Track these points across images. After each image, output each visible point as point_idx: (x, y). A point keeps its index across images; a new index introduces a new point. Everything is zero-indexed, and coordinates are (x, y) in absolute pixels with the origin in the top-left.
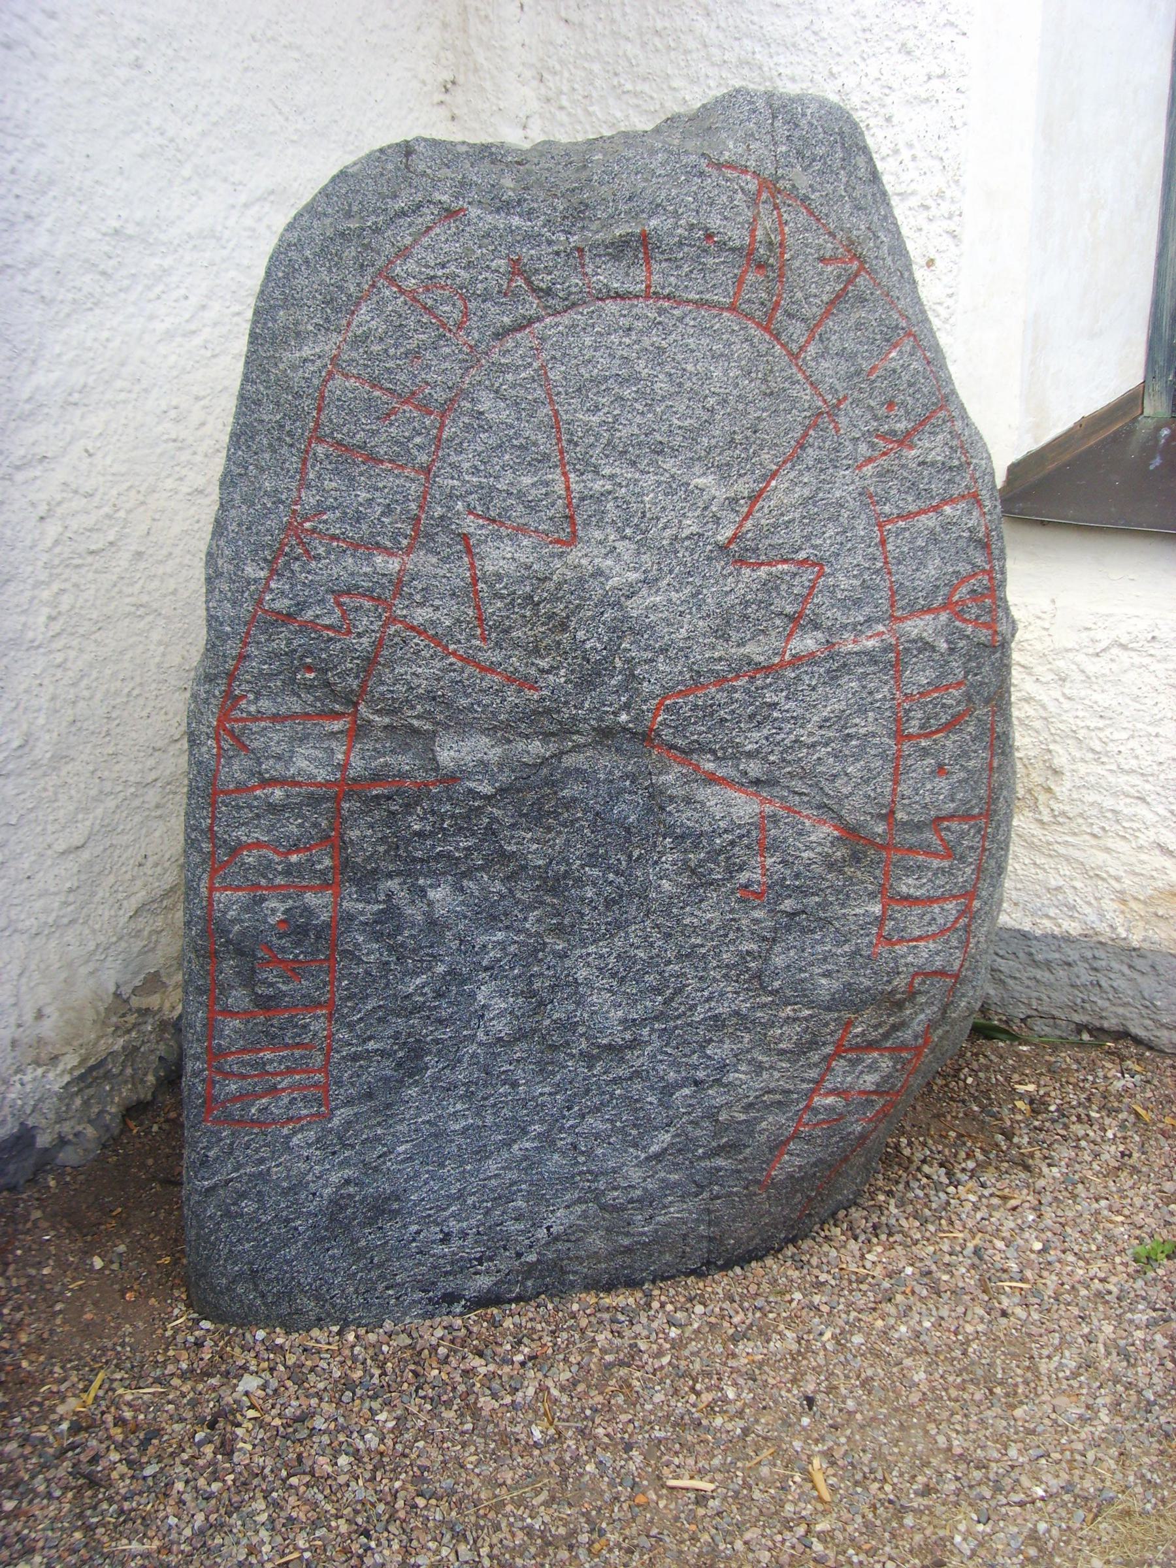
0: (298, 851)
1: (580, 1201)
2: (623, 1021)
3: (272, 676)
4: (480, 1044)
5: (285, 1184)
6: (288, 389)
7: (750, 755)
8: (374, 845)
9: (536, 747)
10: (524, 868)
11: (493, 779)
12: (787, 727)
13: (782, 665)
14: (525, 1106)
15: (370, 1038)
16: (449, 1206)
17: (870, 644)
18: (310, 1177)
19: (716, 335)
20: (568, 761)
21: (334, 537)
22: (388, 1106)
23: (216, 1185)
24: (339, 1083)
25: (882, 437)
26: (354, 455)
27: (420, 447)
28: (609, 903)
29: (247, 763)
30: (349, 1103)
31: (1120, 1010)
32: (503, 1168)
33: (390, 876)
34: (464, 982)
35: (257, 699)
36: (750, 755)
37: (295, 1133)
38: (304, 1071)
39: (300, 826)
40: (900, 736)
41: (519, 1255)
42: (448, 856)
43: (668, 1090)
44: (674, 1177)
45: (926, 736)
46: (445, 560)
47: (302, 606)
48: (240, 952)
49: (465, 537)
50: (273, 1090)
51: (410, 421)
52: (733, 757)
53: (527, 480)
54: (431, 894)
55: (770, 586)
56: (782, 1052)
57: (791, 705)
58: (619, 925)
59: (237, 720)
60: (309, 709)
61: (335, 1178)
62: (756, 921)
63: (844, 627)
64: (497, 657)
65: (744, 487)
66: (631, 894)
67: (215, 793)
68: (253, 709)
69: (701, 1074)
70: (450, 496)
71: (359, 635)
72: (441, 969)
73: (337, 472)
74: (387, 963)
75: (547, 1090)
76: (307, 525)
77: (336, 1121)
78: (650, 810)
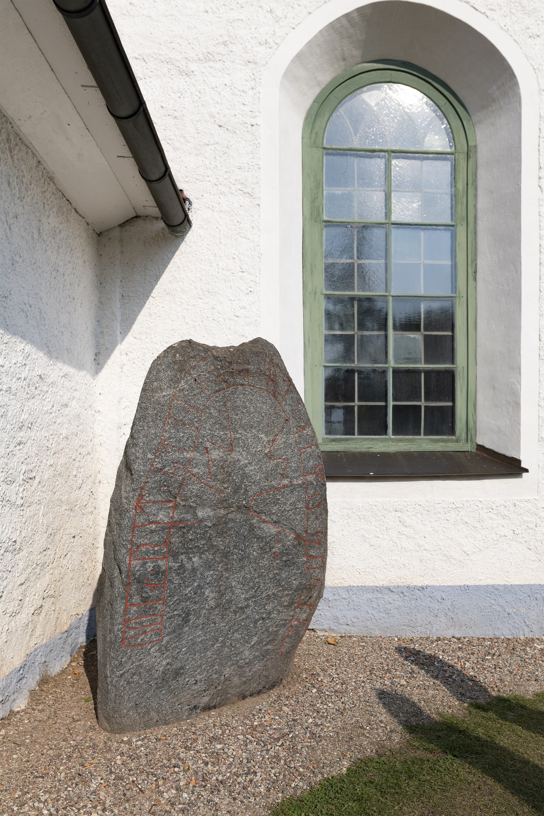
0: (157, 546)
1: (233, 665)
2: (245, 598)
3: (154, 488)
4: (207, 609)
5: (148, 668)
6: (159, 404)
7: (273, 514)
8: (178, 543)
9: (222, 511)
10: (218, 550)
11: (211, 521)
12: (282, 505)
13: (280, 488)
14: (217, 631)
15: (176, 610)
16: (197, 669)
17: (300, 482)
18: (156, 664)
19: (263, 397)
20: (230, 516)
21: (173, 446)
22: (180, 634)
23: (124, 672)
24: (165, 628)
25: (299, 427)
26: (178, 424)
27: (196, 422)
28: (240, 560)
29: (145, 517)
30: (168, 635)
31: (327, 622)
32: (212, 654)
33: (182, 554)
34: (202, 589)
35: (149, 496)
36: (273, 514)
37: (152, 647)
38: (155, 624)
39: (159, 538)
40: (308, 508)
41: (216, 687)
42: (198, 547)
43: (256, 622)
44: (257, 654)
45: (313, 508)
46: (202, 455)
47: (164, 467)
48: (139, 582)
49: (207, 448)
50: (145, 632)
51: (194, 414)
52: (270, 515)
53: (222, 433)
54: (194, 559)
55: (277, 465)
56: (285, 606)
57: (283, 499)
58: (242, 568)
59: (142, 503)
60: (163, 500)
61: (164, 663)
62: (277, 564)
63: (294, 477)
64: (213, 484)
65: (271, 438)
66: (245, 557)
67: (134, 527)
68: (148, 499)
69: (264, 616)
70: (203, 436)
71: (179, 476)
72: (196, 584)
73: (174, 427)
74: (180, 584)
75: (224, 624)
76: (166, 443)
77: (164, 642)
78: (250, 531)
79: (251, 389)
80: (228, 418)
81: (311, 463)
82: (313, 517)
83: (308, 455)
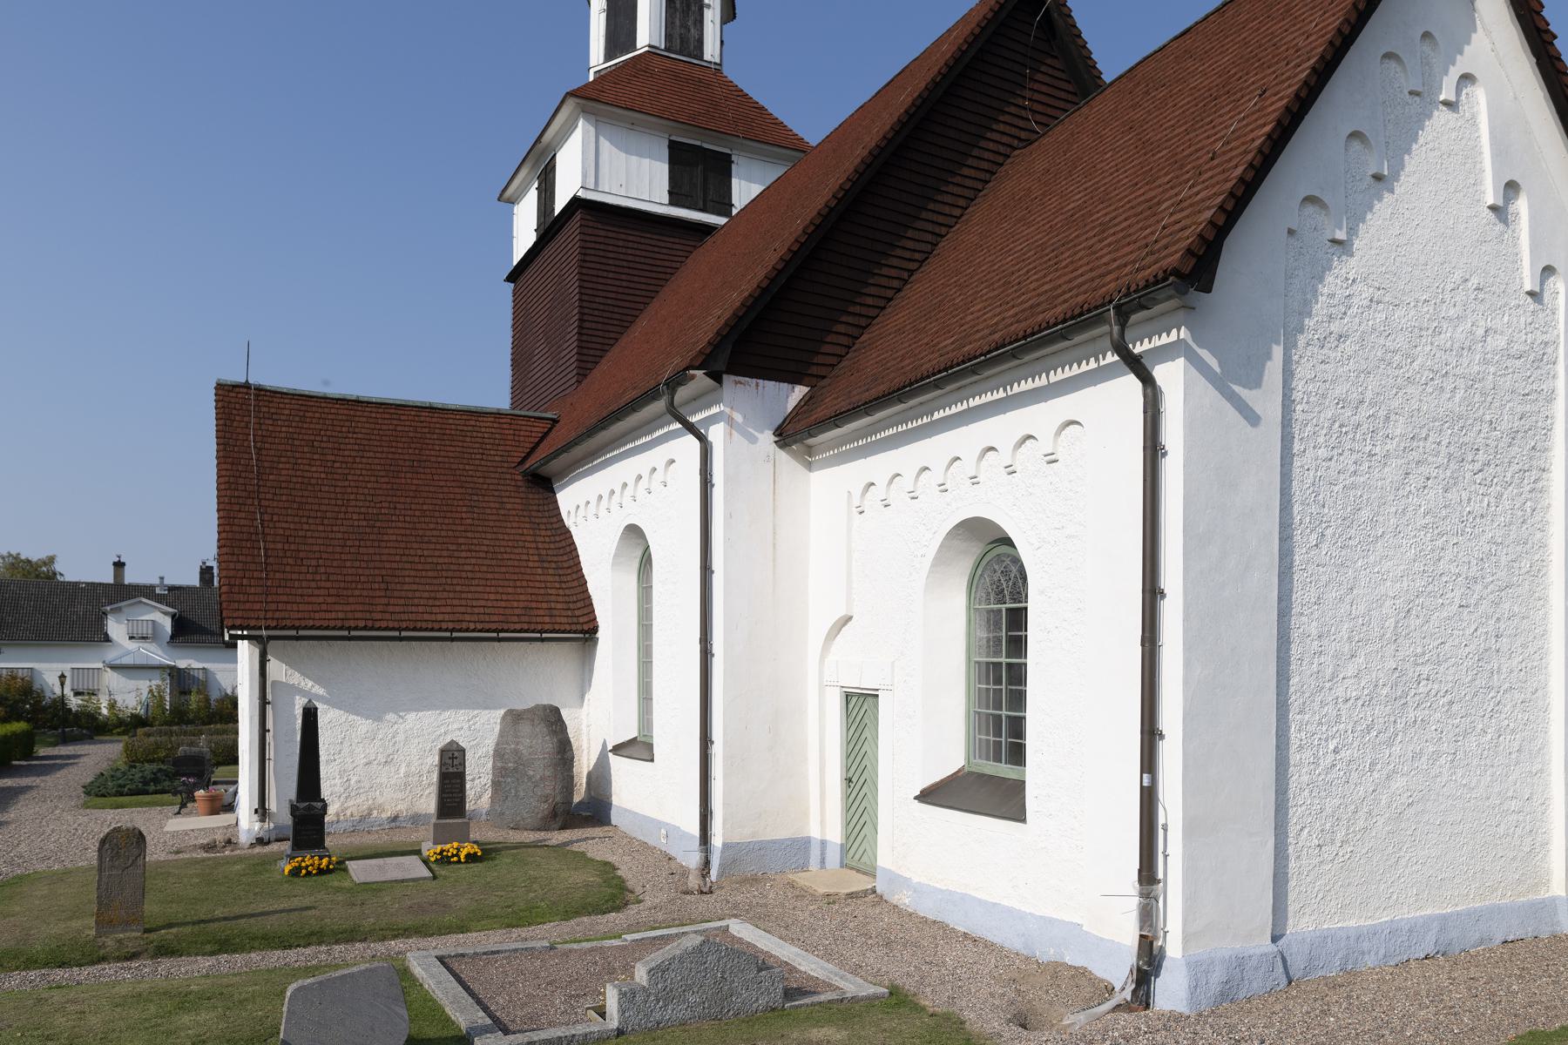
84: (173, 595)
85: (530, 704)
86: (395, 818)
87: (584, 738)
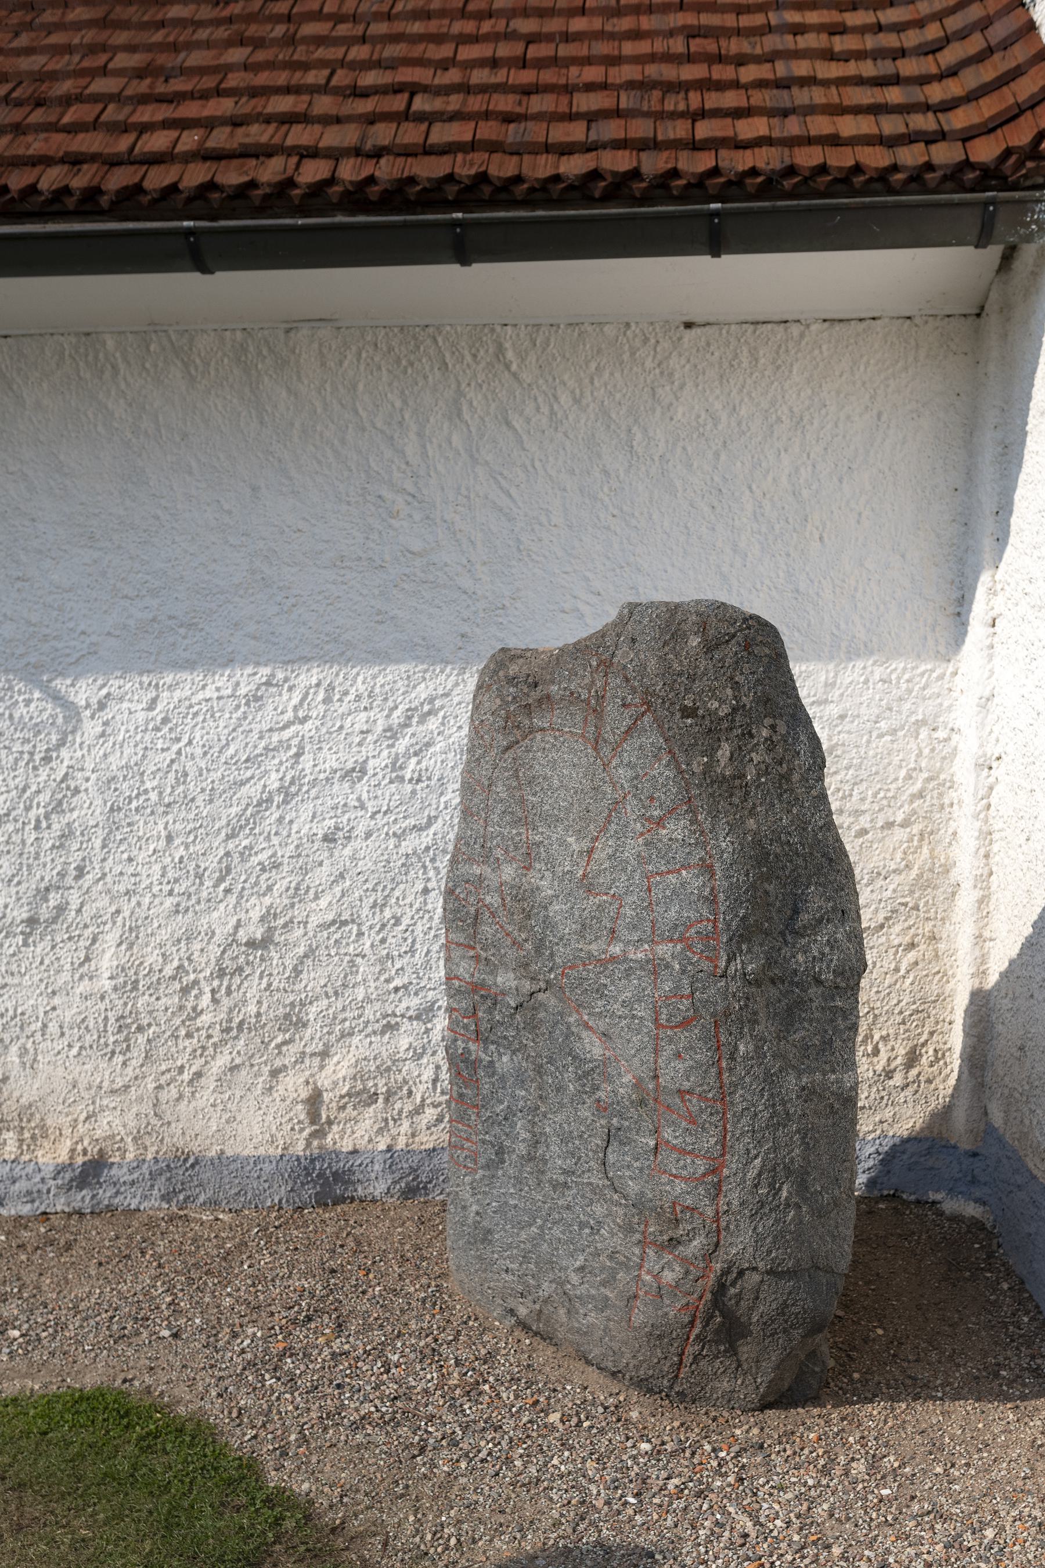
65: (585, 844)
79: (555, 738)
80: (522, 801)
81: (672, 914)
82: (668, 1051)
83: (668, 893)
84: (968, 158)
85: (596, 616)
86: (92, 1171)
87: (964, 825)
